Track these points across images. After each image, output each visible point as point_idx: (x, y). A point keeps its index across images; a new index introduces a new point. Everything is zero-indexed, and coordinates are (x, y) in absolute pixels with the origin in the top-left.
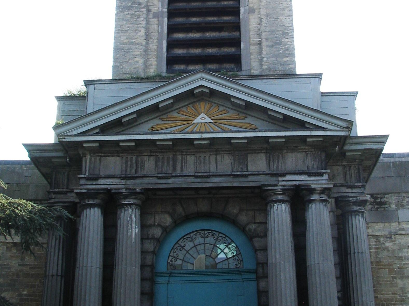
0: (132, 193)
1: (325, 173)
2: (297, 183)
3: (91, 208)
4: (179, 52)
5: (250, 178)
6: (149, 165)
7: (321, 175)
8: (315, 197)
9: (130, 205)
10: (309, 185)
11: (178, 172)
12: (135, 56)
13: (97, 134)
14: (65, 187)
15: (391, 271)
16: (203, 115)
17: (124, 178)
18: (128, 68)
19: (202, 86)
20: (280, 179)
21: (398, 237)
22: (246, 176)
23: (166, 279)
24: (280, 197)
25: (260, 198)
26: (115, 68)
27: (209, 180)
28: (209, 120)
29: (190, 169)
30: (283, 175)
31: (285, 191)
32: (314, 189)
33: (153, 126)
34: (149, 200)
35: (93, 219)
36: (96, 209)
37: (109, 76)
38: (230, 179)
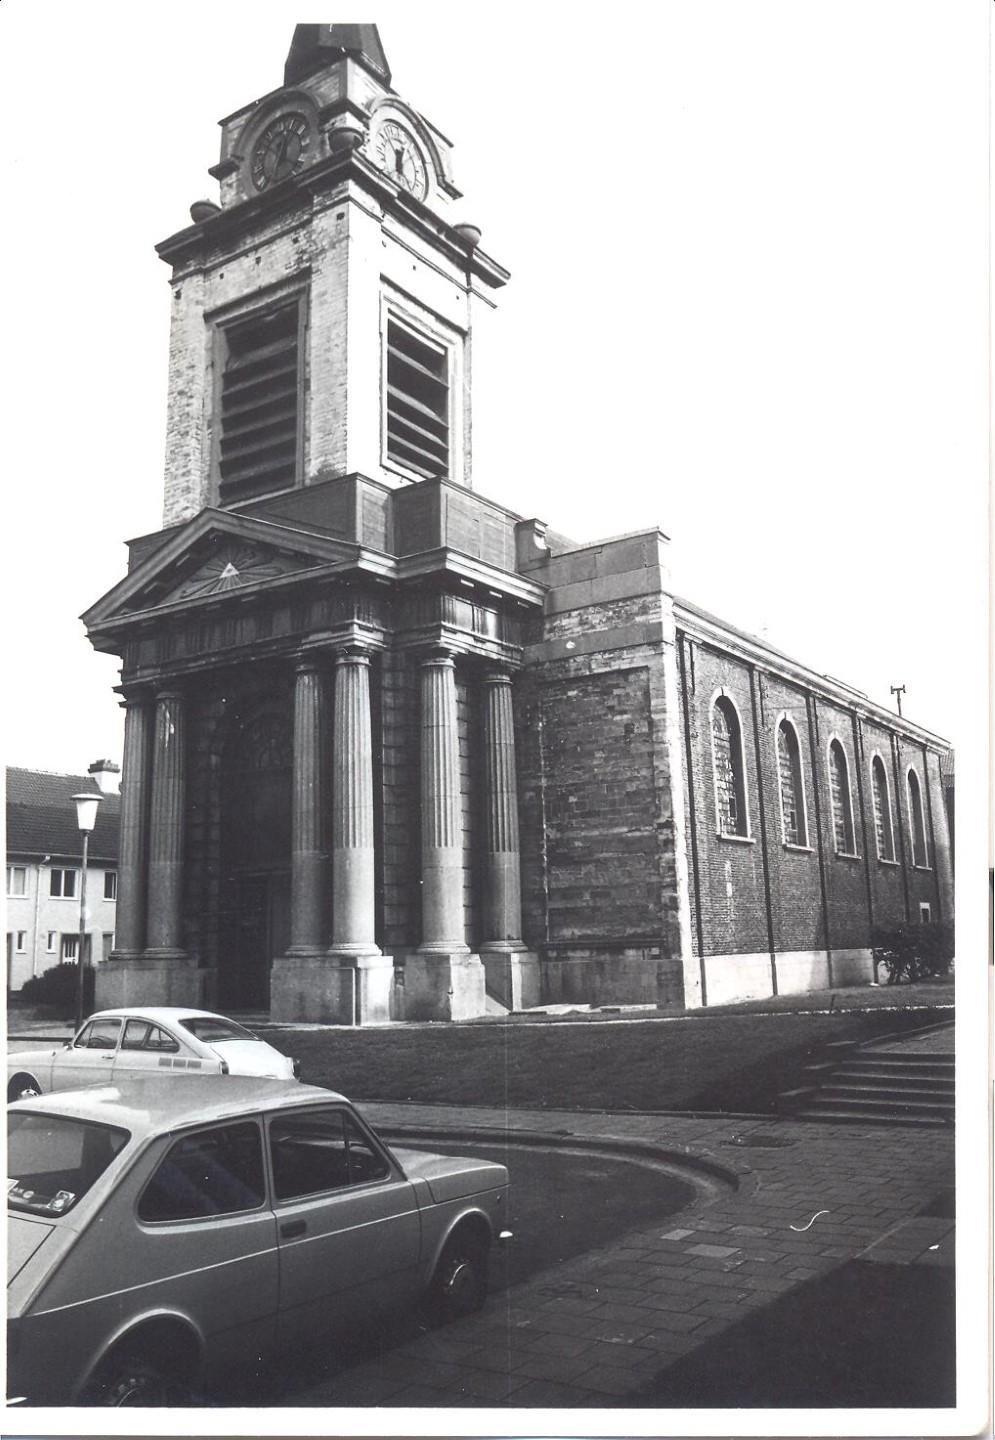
8: (342, 661)
24: (302, 667)
28: (235, 572)
35: (306, 694)
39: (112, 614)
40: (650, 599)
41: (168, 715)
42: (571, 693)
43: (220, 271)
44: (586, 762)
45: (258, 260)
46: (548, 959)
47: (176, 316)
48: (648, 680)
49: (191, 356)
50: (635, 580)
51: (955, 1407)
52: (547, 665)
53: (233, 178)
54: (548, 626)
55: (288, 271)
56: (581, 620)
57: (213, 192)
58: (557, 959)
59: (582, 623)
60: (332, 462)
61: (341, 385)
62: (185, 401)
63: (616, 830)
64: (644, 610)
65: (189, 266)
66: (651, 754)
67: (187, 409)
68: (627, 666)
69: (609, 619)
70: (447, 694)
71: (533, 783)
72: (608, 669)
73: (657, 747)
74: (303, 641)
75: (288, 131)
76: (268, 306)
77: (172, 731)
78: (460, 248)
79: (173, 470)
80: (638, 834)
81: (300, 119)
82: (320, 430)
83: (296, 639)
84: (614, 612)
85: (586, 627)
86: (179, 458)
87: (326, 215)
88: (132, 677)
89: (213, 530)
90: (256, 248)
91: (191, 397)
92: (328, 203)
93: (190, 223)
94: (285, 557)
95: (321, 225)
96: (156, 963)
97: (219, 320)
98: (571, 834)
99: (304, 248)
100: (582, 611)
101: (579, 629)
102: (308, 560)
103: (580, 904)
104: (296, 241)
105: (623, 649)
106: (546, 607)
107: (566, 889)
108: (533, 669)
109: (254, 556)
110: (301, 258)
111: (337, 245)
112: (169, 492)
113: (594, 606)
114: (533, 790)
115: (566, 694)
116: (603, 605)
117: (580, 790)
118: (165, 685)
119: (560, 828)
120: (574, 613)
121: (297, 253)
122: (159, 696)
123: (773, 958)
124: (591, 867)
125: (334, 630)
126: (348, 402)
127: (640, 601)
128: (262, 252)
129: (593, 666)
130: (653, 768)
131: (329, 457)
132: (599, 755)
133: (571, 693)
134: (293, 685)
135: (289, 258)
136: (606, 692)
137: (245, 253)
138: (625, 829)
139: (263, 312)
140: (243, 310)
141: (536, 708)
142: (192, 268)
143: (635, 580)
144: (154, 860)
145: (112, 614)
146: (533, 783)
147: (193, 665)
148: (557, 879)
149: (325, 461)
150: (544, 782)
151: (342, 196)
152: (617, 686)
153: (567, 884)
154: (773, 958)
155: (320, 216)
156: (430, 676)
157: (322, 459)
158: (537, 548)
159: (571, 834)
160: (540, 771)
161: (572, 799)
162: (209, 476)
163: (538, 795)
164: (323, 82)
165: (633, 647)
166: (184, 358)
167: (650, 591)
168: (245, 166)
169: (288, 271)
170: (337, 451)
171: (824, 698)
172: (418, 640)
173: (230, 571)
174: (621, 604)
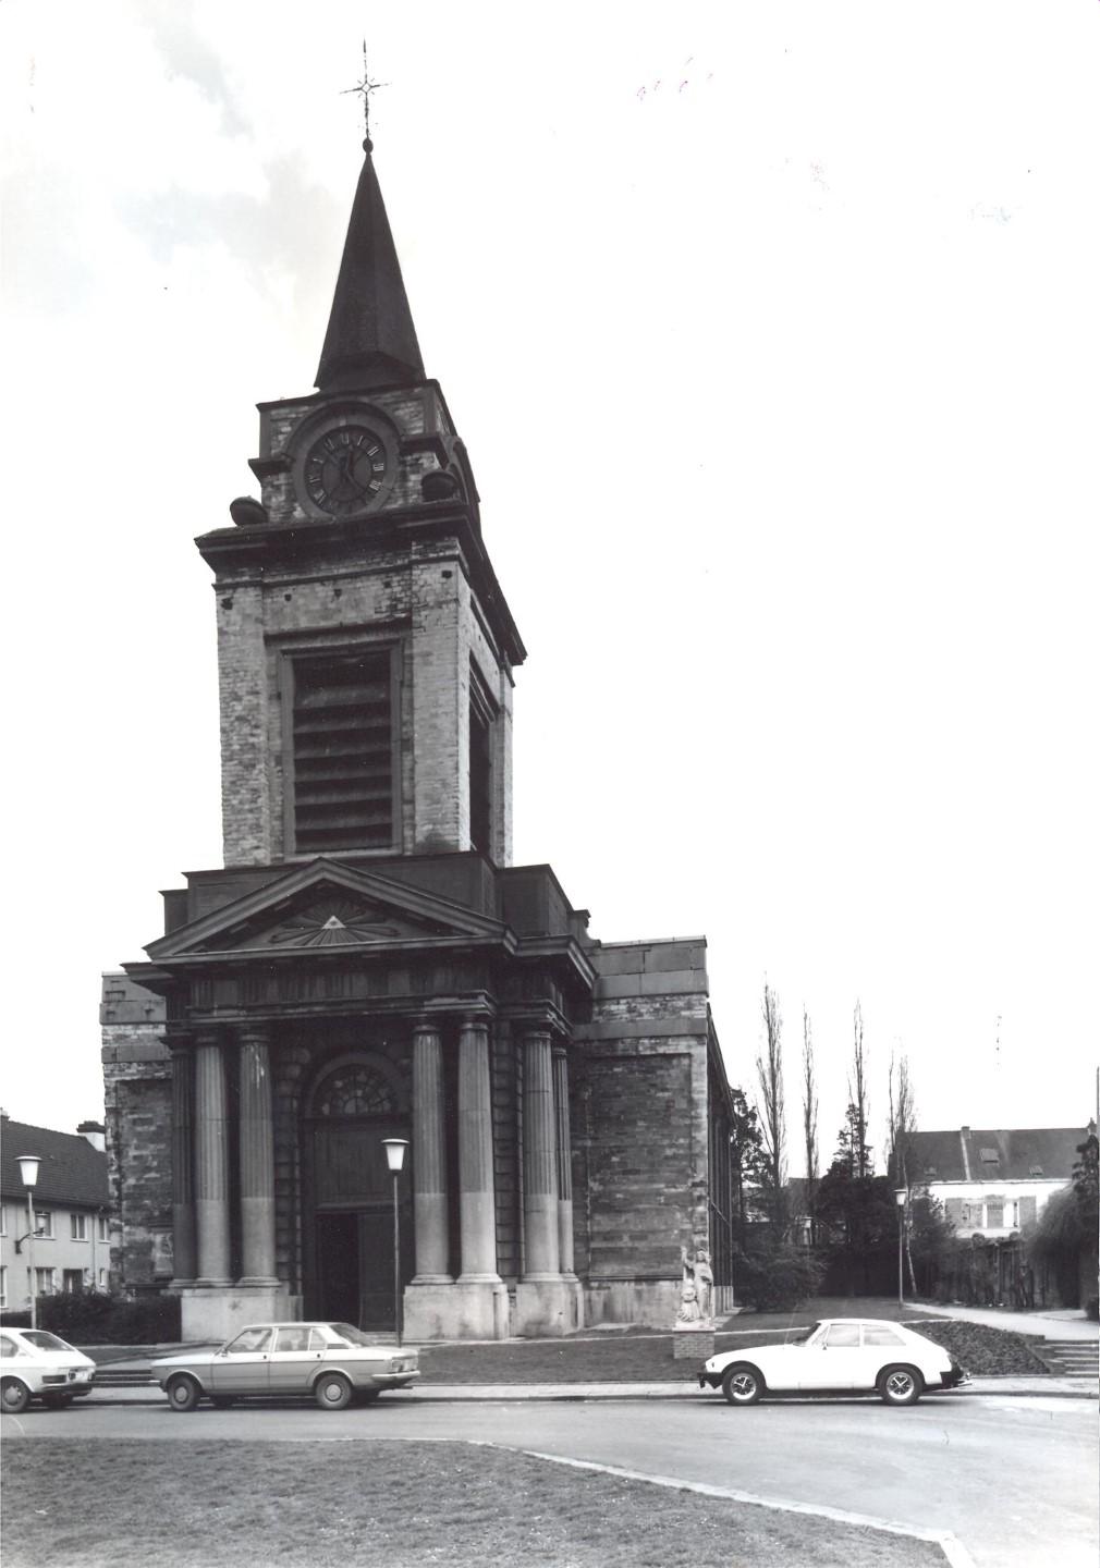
1: (480, 994)
3: (88, 1222)
5: (344, 1007)
6: (272, 992)
9: (252, 1042)
14: (397, 1369)
16: (333, 918)
24: (424, 1028)
25: (405, 1032)
28: (340, 925)
33: (274, 937)
34: (279, 1037)
35: (427, 1051)
39: (187, 950)
40: (695, 997)
41: (257, 1058)
42: (616, 1070)
43: (289, 591)
44: (628, 1129)
45: (338, 593)
46: (591, 1289)
47: (225, 629)
48: (690, 1066)
49: (252, 680)
50: (684, 980)
52: (596, 1044)
53: (282, 479)
54: (596, 1009)
55: (378, 616)
56: (629, 1007)
57: (253, 489)
58: (599, 1288)
59: (630, 1011)
60: (441, 832)
61: (451, 756)
62: (246, 730)
63: (656, 1186)
64: (689, 1007)
65: (243, 574)
66: (691, 1126)
67: (252, 740)
68: (671, 1052)
69: (657, 1010)
72: (654, 1052)
73: (695, 1121)
74: (426, 1003)
75: (354, 447)
76: (349, 647)
77: (263, 1073)
79: (235, 802)
80: (673, 1190)
81: (373, 438)
82: (427, 796)
83: (419, 1001)
84: (661, 1005)
85: (635, 1014)
86: (243, 791)
87: (429, 568)
88: (208, 1015)
89: (323, 880)
90: (335, 579)
91: (257, 727)
92: (431, 555)
93: (228, 523)
95: (423, 576)
96: (264, 1290)
97: (285, 647)
98: (613, 1187)
99: (398, 596)
100: (630, 1000)
101: (627, 1015)
102: (446, 930)
103: (620, 1244)
104: (388, 585)
105: (669, 1036)
106: (596, 989)
107: (609, 1232)
108: (582, 1045)
109: (363, 913)
110: (396, 606)
111: (444, 606)
112: (230, 826)
113: (642, 997)
115: (611, 1069)
116: (651, 997)
117: (623, 1151)
118: (256, 1028)
119: (602, 1182)
120: (623, 1001)
121: (388, 599)
124: (630, 1216)
125: (461, 997)
126: (459, 775)
127: (687, 998)
128: (341, 585)
129: (641, 1048)
130: (692, 1138)
131: (438, 827)
132: (641, 1123)
133: (616, 1070)
135: (380, 602)
136: (652, 1070)
137: (322, 580)
138: (662, 1186)
139: (342, 653)
140: (318, 644)
141: (583, 1079)
142: (246, 578)
143: (684, 980)
144: (206, 1198)
145: (187, 950)
147: (291, 1011)
148: (599, 1224)
149: (433, 829)
151: (448, 553)
152: (661, 1068)
153: (608, 1229)
155: (421, 567)
156: (536, 1045)
157: (431, 827)
158: (588, 938)
159: (613, 1187)
160: (585, 1133)
161: (614, 1159)
162: (281, 818)
164: (403, 405)
165: (679, 1036)
166: (242, 681)
167: (696, 990)
168: (299, 468)
169: (378, 616)
170: (448, 823)
172: (521, 1013)
173: (333, 923)
174: (667, 998)
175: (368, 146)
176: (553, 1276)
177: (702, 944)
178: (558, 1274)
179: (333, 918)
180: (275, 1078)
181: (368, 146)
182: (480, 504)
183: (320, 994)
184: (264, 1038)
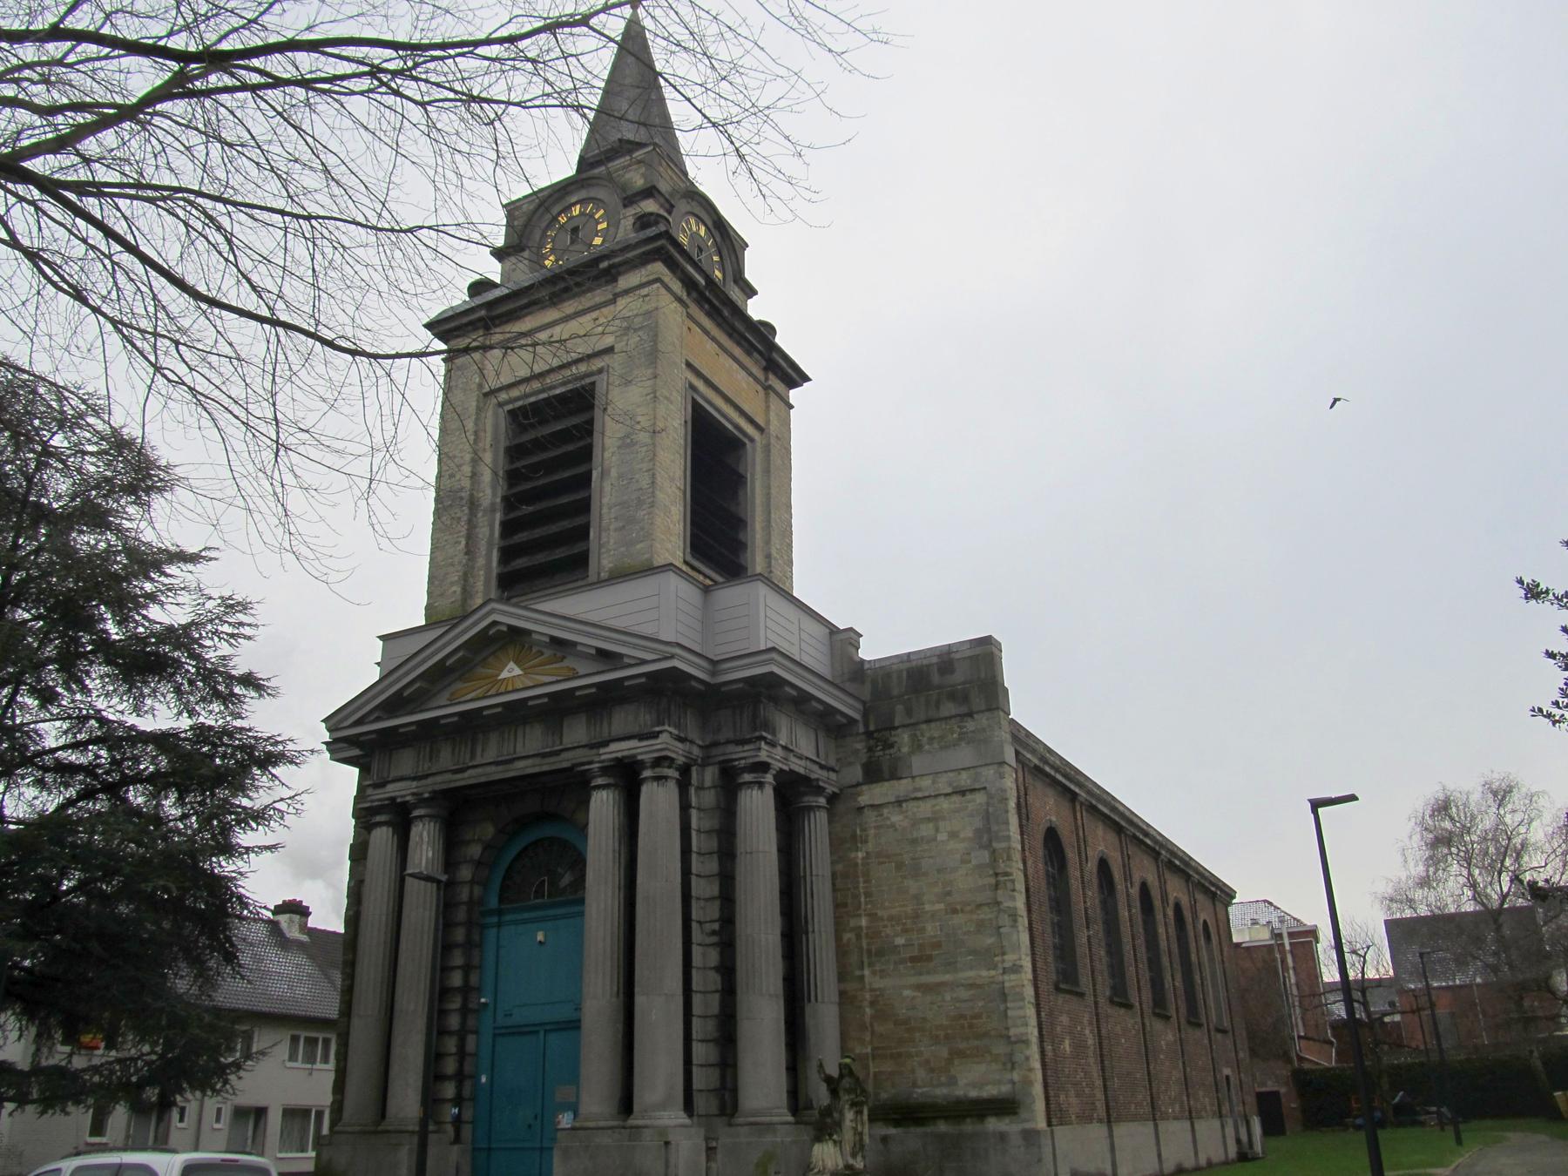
0: (421, 802)
2: (619, 755)
4: (521, 563)
5: (565, 755)
7: (656, 735)
8: (647, 773)
10: (634, 756)
11: (479, 760)
12: (452, 584)
13: (378, 719)
15: (900, 866)
17: (413, 779)
18: (434, 619)
19: (495, 623)
20: (602, 751)
21: (912, 804)
22: (557, 753)
23: (495, 919)
24: (600, 781)
25: (570, 787)
26: (429, 609)
27: (511, 766)
28: (518, 671)
29: (491, 754)
30: (606, 744)
31: (605, 771)
32: (642, 762)
35: (603, 806)
36: (384, 829)
37: (423, 623)
38: (537, 761)
51: (985, 653)
57: (493, 270)
70: (758, 809)
71: (853, 923)
78: (758, 343)
94: (585, 656)
114: (852, 930)
122: (416, 813)
123: (1156, 1126)
134: (585, 802)
146: (853, 923)
150: (864, 922)
154: (1156, 1126)
163: (859, 937)
171: (1135, 837)
173: (511, 671)
175: (1533, 592)
176: (674, 1117)
177: (985, 653)
178: (682, 1114)
179: (511, 665)
180: (450, 859)
181: (1533, 592)
182: (779, 340)
183: (491, 754)
184: (611, 781)
